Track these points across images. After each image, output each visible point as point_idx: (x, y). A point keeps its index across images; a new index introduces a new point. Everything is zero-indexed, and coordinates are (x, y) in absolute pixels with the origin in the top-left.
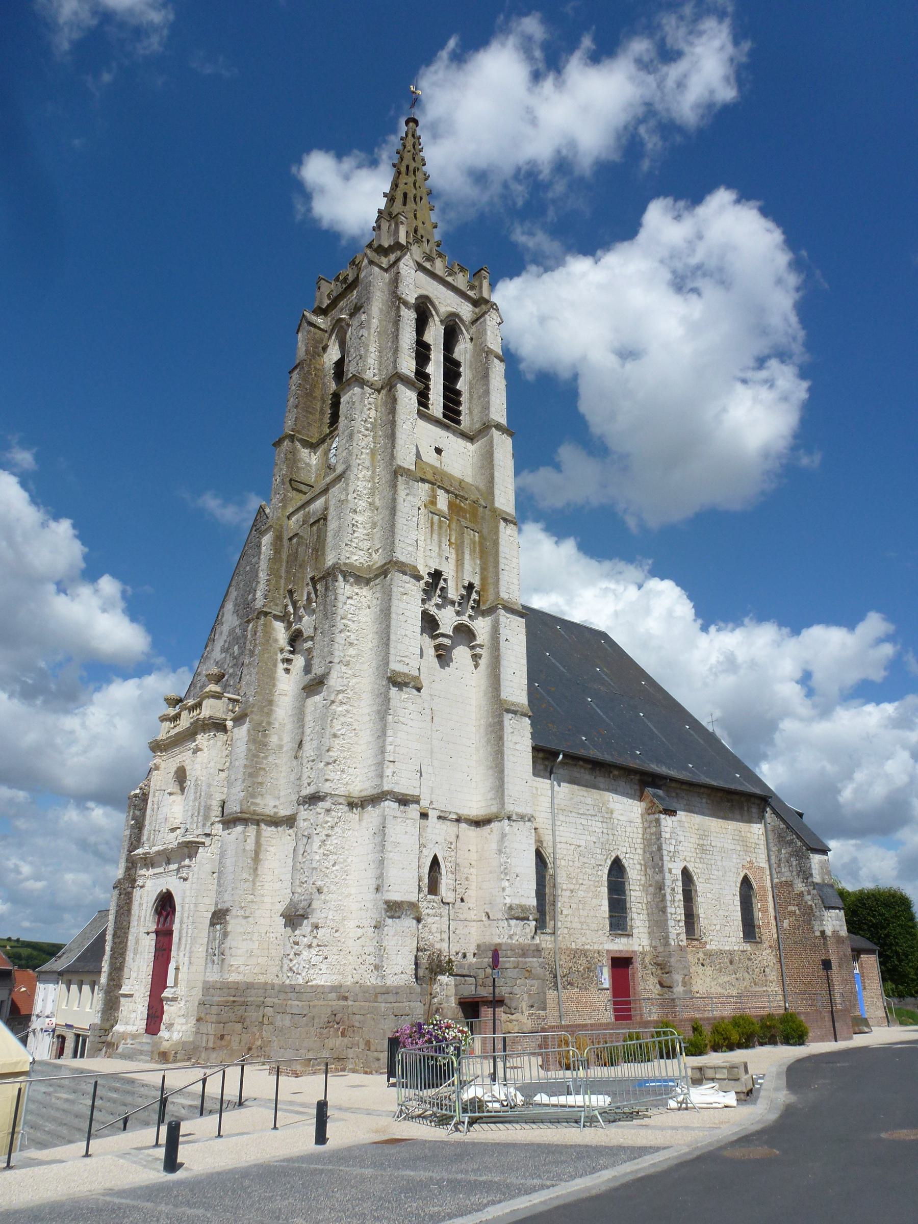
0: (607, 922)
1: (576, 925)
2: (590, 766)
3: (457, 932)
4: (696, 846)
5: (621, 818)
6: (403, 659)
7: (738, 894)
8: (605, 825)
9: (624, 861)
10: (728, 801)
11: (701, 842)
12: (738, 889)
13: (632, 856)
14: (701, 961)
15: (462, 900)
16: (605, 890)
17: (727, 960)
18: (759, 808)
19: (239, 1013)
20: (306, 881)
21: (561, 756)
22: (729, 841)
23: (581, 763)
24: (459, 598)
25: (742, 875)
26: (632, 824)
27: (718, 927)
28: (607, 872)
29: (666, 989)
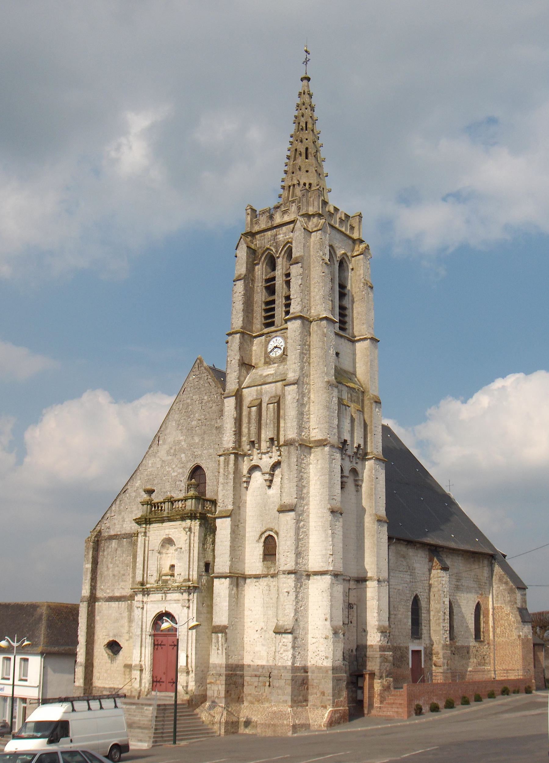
0: (410, 631)
1: (397, 633)
2: (406, 543)
3: (349, 639)
4: (454, 586)
5: (419, 572)
6: (334, 497)
7: (474, 613)
8: (411, 577)
9: (419, 597)
10: (472, 558)
11: (457, 583)
12: (474, 611)
13: (423, 594)
14: (453, 652)
15: (351, 623)
16: (410, 613)
17: (466, 651)
18: (488, 561)
19: (234, 680)
20: (288, 615)
21: (395, 540)
22: (471, 582)
23: (402, 542)
24: (353, 453)
25: (477, 602)
26: (424, 575)
27: (463, 633)
28: (411, 603)
29: (438, 667)
